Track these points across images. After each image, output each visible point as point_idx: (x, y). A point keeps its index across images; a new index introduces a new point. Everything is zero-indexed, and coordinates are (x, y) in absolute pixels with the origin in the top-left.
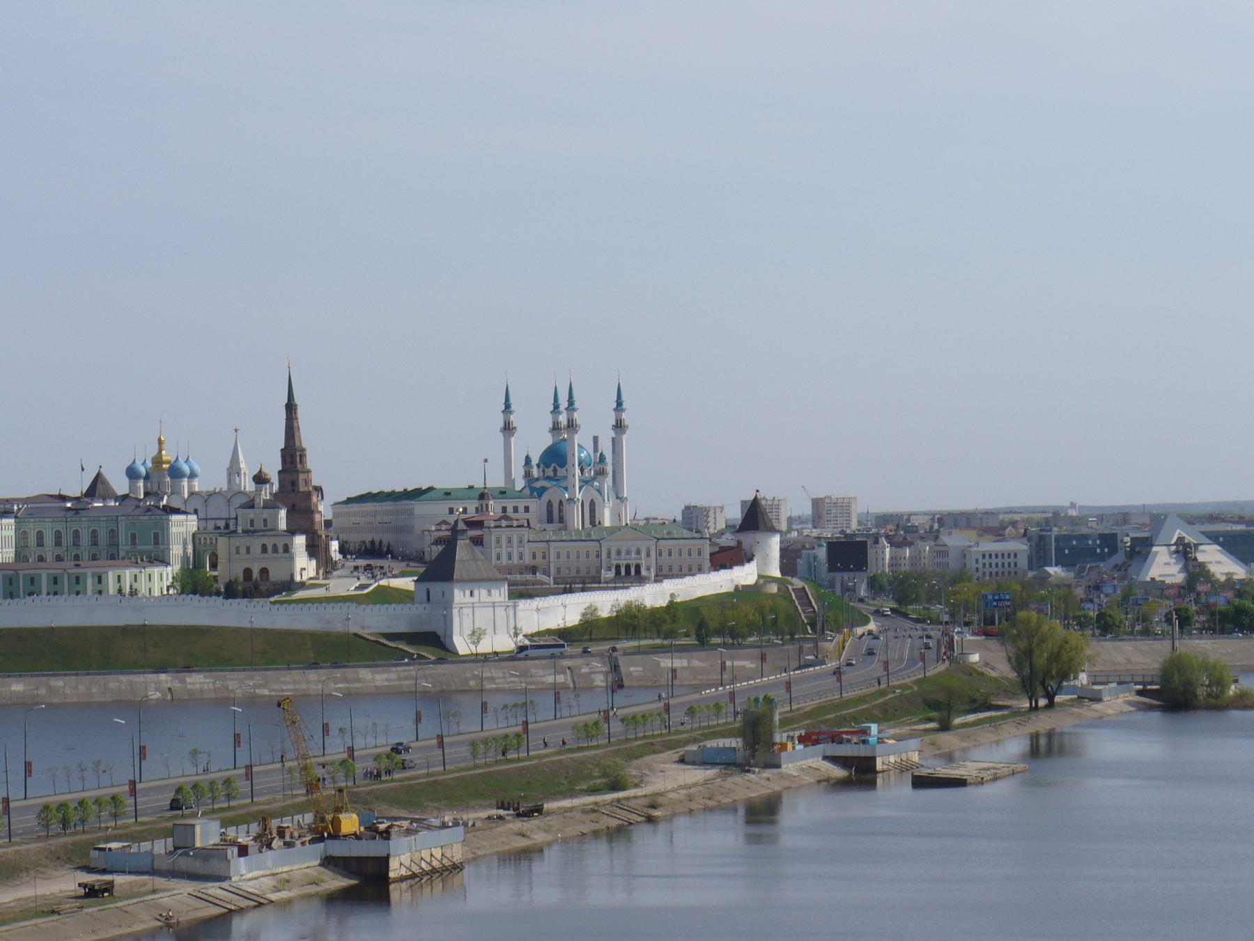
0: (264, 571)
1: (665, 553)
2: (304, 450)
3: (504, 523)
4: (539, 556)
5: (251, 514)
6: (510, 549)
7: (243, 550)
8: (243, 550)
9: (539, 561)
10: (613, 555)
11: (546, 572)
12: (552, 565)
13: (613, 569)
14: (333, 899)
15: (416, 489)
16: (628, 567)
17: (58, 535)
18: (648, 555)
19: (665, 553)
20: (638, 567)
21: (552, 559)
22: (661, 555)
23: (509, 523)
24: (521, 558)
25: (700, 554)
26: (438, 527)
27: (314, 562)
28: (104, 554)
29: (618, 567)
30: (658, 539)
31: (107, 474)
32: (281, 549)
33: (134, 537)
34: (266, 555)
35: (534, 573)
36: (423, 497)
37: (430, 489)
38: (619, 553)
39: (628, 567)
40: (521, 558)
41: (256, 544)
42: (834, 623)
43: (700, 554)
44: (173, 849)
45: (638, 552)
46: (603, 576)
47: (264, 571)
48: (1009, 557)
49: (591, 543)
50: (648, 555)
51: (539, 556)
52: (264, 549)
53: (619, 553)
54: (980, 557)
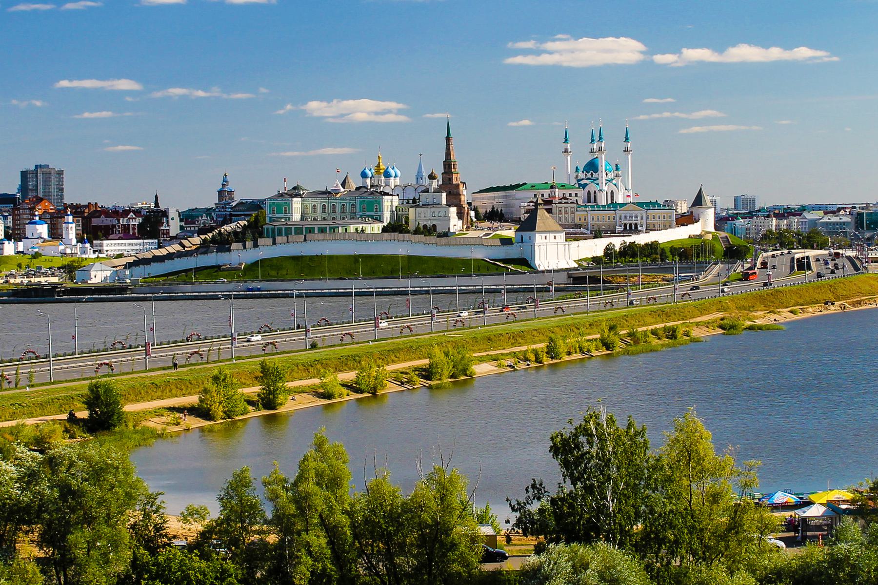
12: (589, 224)
16: (631, 225)
18: (642, 218)
20: (636, 225)
23: (566, 201)
29: (625, 225)
39: (631, 225)
50: (642, 218)
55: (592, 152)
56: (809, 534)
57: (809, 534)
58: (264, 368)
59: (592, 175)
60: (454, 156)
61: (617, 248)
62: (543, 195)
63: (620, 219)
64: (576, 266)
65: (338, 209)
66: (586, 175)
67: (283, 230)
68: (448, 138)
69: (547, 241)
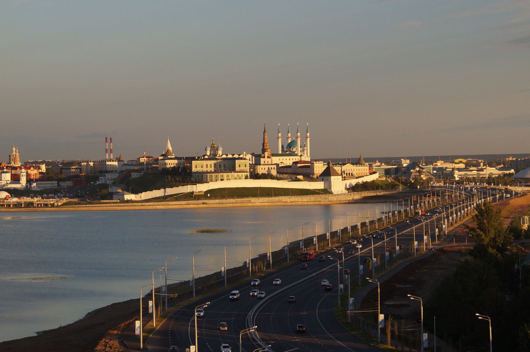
7: (263, 169)
8: (263, 169)
29: (347, 173)
39: (349, 173)
45: (351, 170)
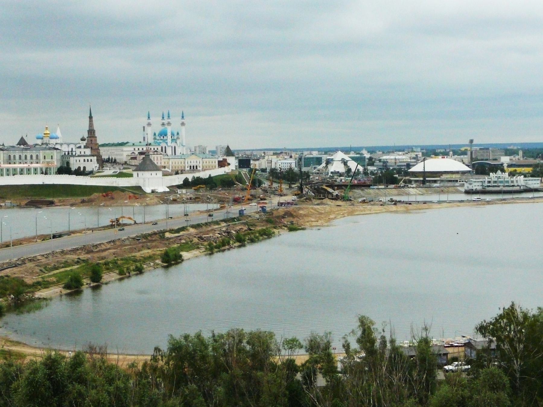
0: (84, 168)
1: (205, 162)
2: (95, 131)
3: (155, 153)
4: (166, 163)
5: (79, 150)
6: (157, 161)
7: (78, 161)
8: (78, 161)
9: (166, 165)
10: (189, 162)
11: (169, 168)
12: (170, 166)
13: (189, 167)
14: (68, 295)
15: (122, 143)
16: (193, 167)
17: (20, 156)
18: (200, 163)
19: (205, 162)
20: (196, 166)
21: (170, 164)
22: (203, 163)
23: (157, 153)
24: (161, 163)
25: (215, 162)
26: (154, 153)
27: (98, 165)
28: (17, 162)
29: (190, 167)
30: (203, 158)
31: (23, 137)
32: (90, 161)
33: (45, 157)
34: (85, 163)
35: (165, 168)
36: (126, 145)
37: (127, 143)
38: (191, 162)
39: (193, 167)
40: (161, 163)
41: (82, 159)
42: (399, 381)
43: (215, 162)
44: (151, 192)
46: (186, 169)
47: (84, 168)
48: (286, 164)
49: (182, 159)
50: (200, 163)
51: (166, 163)
52: (84, 160)
53: (191, 162)
54: (281, 164)
55: (163, 124)
56: (427, 179)
57: (427, 179)
58: (395, 158)
59: (163, 137)
60: (96, 127)
61: (190, 180)
62: (139, 149)
63: (188, 163)
64: (168, 190)
65: (29, 158)
66: (160, 137)
67: (11, 169)
68: (91, 117)
69: (152, 176)
